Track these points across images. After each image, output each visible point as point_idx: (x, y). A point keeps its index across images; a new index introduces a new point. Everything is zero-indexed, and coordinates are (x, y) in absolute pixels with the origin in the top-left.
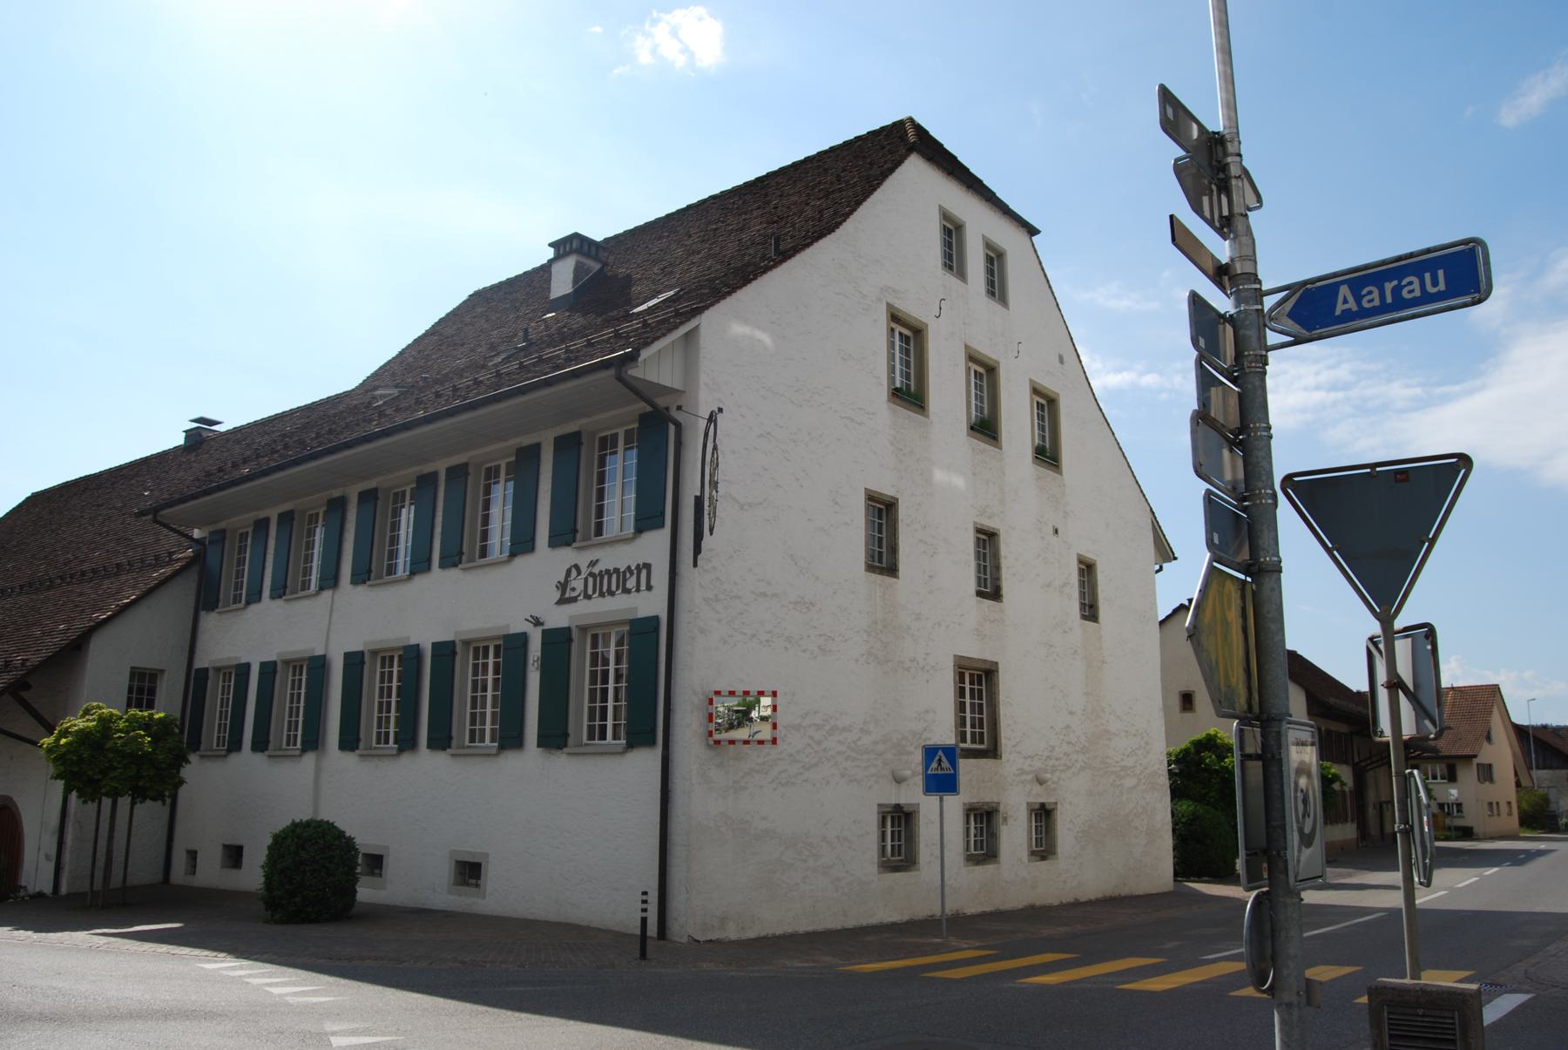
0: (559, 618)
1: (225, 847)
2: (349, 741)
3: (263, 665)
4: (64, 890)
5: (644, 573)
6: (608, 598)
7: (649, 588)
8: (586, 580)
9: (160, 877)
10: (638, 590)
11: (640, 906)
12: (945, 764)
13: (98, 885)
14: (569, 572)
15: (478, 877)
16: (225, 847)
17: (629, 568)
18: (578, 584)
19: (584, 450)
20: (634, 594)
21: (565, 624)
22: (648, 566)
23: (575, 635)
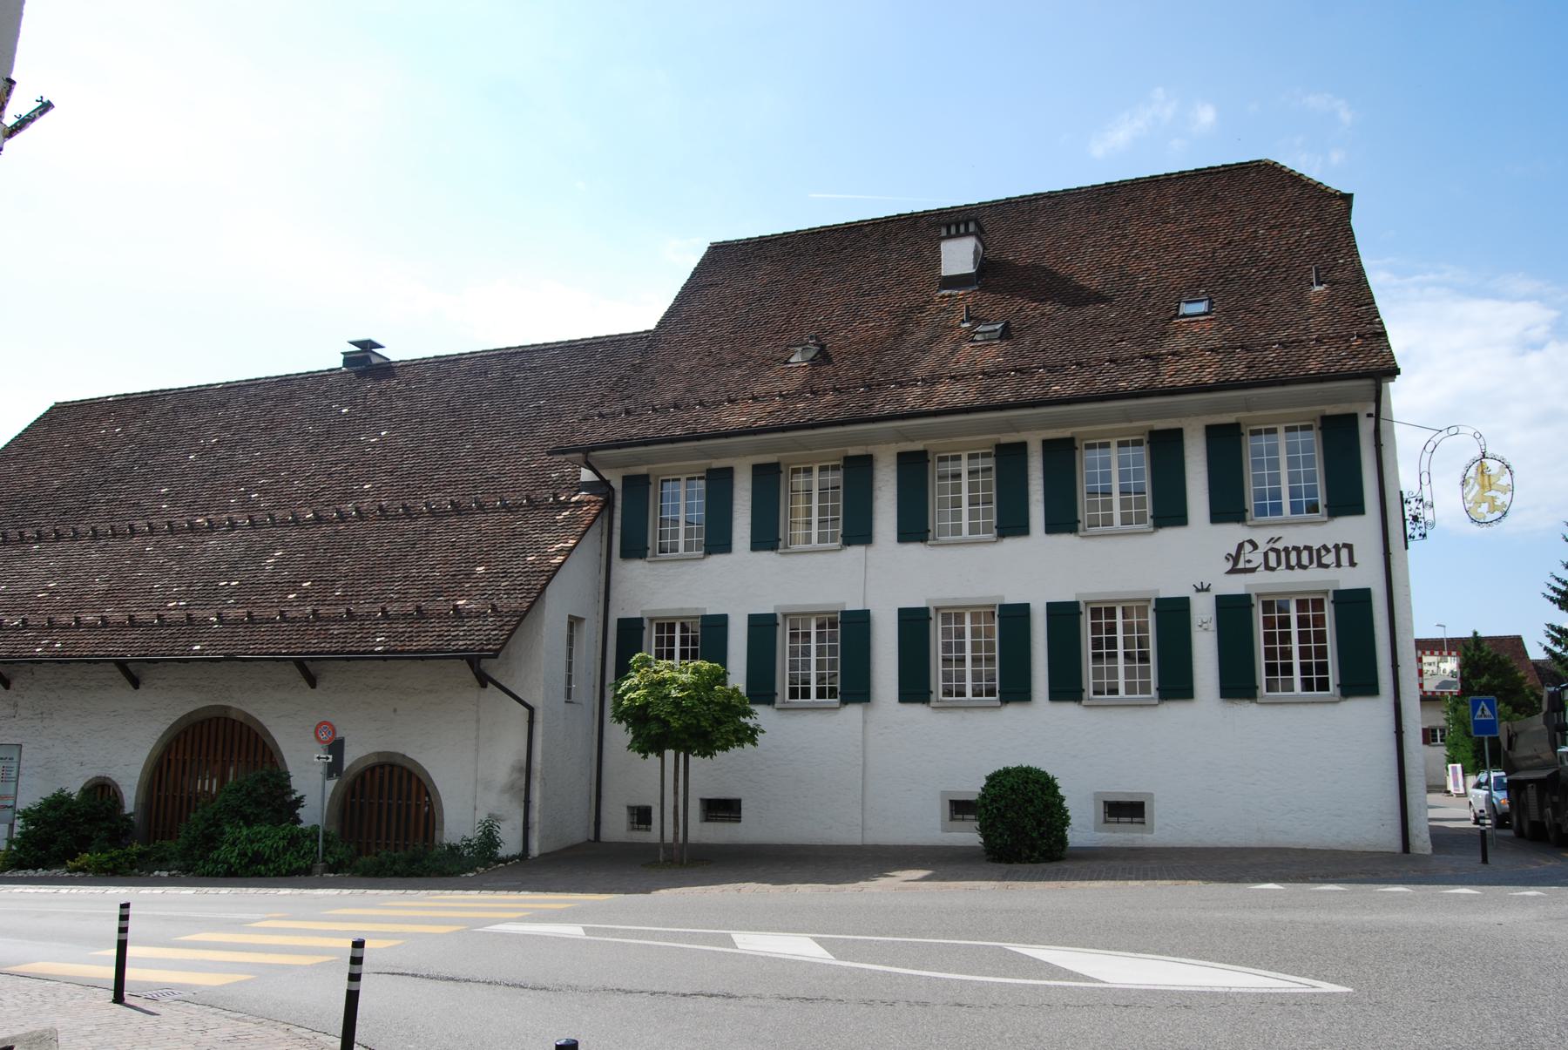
0: (1236, 586)
1: (631, 808)
2: (914, 688)
3: (1054, 609)
4: (535, 850)
5: (1344, 553)
6: (1298, 571)
7: (1352, 564)
8: (1266, 554)
9: (592, 837)
10: (1339, 565)
11: (116, 924)
12: (1487, 712)
13: (669, 837)
14: (1241, 546)
15: (1142, 816)
16: (631, 808)
17: (1325, 547)
18: (1257, 558)
19: (651, 488)
20: (1333, 569)
21: (771, 611)
22: (1349, 547)
23: (780, 620)
